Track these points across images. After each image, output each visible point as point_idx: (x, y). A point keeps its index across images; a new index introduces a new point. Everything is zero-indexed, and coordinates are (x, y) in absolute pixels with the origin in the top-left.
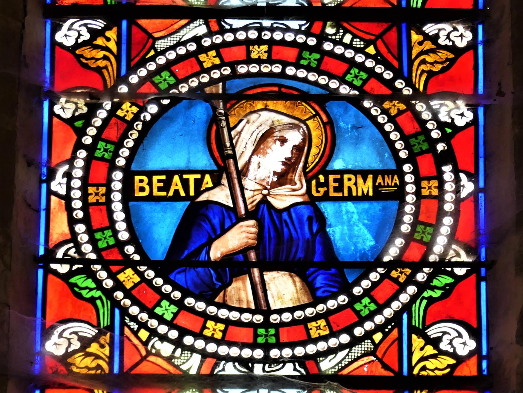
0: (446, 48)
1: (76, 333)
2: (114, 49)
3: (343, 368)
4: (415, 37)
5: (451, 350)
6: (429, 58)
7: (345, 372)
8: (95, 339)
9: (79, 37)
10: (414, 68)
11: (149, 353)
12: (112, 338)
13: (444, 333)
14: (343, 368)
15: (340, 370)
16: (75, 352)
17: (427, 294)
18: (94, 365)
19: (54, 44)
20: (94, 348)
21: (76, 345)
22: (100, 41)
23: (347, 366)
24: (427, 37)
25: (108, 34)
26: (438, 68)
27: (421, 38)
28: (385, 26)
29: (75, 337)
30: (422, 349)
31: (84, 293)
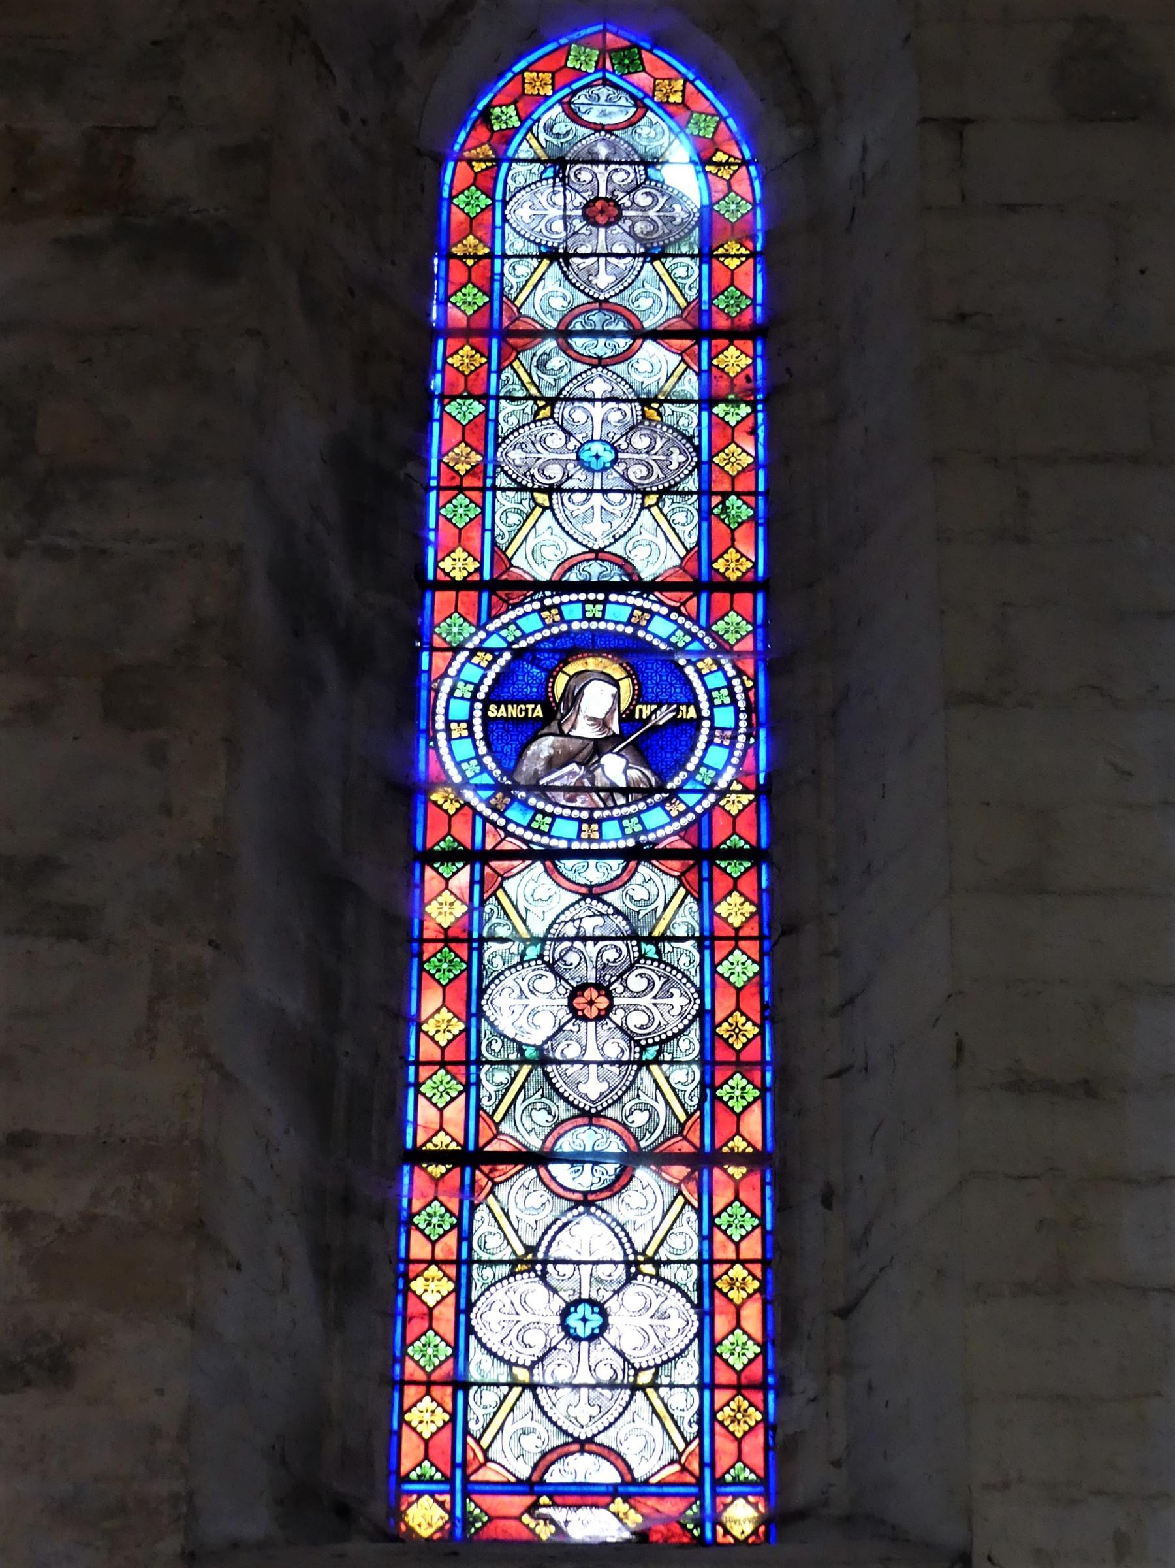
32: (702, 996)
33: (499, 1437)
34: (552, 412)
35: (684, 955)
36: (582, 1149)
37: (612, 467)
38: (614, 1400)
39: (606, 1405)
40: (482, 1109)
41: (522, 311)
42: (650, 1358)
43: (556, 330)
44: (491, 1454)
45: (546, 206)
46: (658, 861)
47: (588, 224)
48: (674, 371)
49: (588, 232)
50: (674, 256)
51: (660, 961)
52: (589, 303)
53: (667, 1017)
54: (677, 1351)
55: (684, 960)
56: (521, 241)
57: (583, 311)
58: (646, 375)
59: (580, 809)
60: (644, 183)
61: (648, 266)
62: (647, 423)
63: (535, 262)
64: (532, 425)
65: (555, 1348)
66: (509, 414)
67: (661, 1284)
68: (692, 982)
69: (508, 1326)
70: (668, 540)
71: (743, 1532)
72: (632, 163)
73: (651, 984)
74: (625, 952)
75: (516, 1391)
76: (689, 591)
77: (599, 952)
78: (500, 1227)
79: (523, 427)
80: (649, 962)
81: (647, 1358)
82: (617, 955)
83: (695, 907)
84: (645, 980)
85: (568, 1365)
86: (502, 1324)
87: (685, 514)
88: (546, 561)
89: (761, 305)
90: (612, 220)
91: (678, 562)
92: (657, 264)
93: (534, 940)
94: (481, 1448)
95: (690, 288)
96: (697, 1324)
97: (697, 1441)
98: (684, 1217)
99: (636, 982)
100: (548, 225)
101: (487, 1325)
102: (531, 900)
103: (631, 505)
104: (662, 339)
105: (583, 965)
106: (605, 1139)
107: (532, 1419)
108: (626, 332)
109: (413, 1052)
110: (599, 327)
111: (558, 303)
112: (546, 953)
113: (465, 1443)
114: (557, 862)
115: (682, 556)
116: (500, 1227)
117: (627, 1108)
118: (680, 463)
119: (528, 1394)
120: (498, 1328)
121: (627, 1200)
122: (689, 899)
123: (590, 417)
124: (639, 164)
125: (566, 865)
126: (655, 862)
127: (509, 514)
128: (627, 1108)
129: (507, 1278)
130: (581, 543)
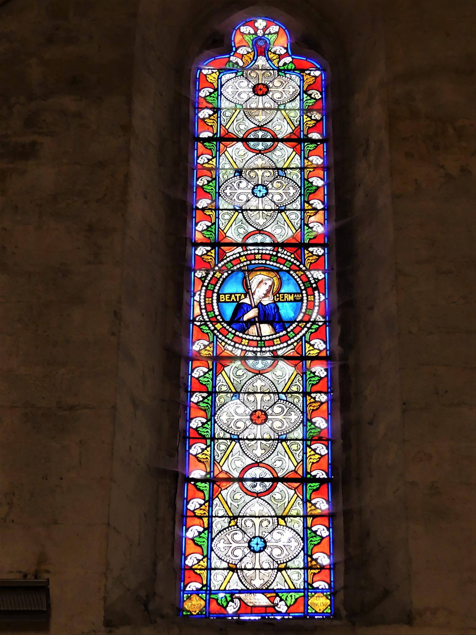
0: (314, 120)
1: (202, 343)
2: (214, 256)
3: (285, 354)
4: (306, 252)
5: (318, 348)
6: (313, 457)
7: (285, 355)
9: (202, 275)
10: (306, 261)
11: (225, 350)
14: (285, 354)
15: (284, 354)
17: (310, 331)
23: (286, 353)
27: (306, 96)
28: (297, 248)
31: (205, 331)
32: (301, 190)
33: (230, 229)
35: (296, 523)
36: (255, 477)
37: (266, 196)
38: (269, 577)
40: (220, 228)
41: (223, 468)
45: (234, 414)
46: (286, 483)
47: (255, 94)
48: (290, 155)
50: (290, 210)
52: (254, 231)
53: (290, 551)
54: (295, 555)
56: (223, 432)
57: (253, 130)
58: (279, 157)
60: (278, 401)
61: (279, 573)
62: (279, 177)
67: (287, 528)
68: (299, 409)
70: (289, 458)
71: (320, 610)
73: (283, 410)
74: (272, 173)
77: (260, 522)
80: (282, 77)
81: (283, 559)
82: (270, 398)
83: (299, 158)
84: (281, 409)
85: (251, 563)
86: (225, 548)
87: (295, 215)
90: (264, 93)
92: (283, 213)
95: (296, 121)
96: (302, 544)
97: (300, 229)
99: (277, 409)
101: (219, 549)
102: (235, 375)
103: (273, 523)
104: (286, 142)
105: (257, 177)
106: (264, 473)
107: (237, 586)
108: (272, 357)
110: (259, 483)
114: (244, 482)
120: (223, 550)
121: (275, 153)
122: (297, 155)
123: (257, 175)
124: (274, 517)
127: (225, 215)
130: (254, 123)
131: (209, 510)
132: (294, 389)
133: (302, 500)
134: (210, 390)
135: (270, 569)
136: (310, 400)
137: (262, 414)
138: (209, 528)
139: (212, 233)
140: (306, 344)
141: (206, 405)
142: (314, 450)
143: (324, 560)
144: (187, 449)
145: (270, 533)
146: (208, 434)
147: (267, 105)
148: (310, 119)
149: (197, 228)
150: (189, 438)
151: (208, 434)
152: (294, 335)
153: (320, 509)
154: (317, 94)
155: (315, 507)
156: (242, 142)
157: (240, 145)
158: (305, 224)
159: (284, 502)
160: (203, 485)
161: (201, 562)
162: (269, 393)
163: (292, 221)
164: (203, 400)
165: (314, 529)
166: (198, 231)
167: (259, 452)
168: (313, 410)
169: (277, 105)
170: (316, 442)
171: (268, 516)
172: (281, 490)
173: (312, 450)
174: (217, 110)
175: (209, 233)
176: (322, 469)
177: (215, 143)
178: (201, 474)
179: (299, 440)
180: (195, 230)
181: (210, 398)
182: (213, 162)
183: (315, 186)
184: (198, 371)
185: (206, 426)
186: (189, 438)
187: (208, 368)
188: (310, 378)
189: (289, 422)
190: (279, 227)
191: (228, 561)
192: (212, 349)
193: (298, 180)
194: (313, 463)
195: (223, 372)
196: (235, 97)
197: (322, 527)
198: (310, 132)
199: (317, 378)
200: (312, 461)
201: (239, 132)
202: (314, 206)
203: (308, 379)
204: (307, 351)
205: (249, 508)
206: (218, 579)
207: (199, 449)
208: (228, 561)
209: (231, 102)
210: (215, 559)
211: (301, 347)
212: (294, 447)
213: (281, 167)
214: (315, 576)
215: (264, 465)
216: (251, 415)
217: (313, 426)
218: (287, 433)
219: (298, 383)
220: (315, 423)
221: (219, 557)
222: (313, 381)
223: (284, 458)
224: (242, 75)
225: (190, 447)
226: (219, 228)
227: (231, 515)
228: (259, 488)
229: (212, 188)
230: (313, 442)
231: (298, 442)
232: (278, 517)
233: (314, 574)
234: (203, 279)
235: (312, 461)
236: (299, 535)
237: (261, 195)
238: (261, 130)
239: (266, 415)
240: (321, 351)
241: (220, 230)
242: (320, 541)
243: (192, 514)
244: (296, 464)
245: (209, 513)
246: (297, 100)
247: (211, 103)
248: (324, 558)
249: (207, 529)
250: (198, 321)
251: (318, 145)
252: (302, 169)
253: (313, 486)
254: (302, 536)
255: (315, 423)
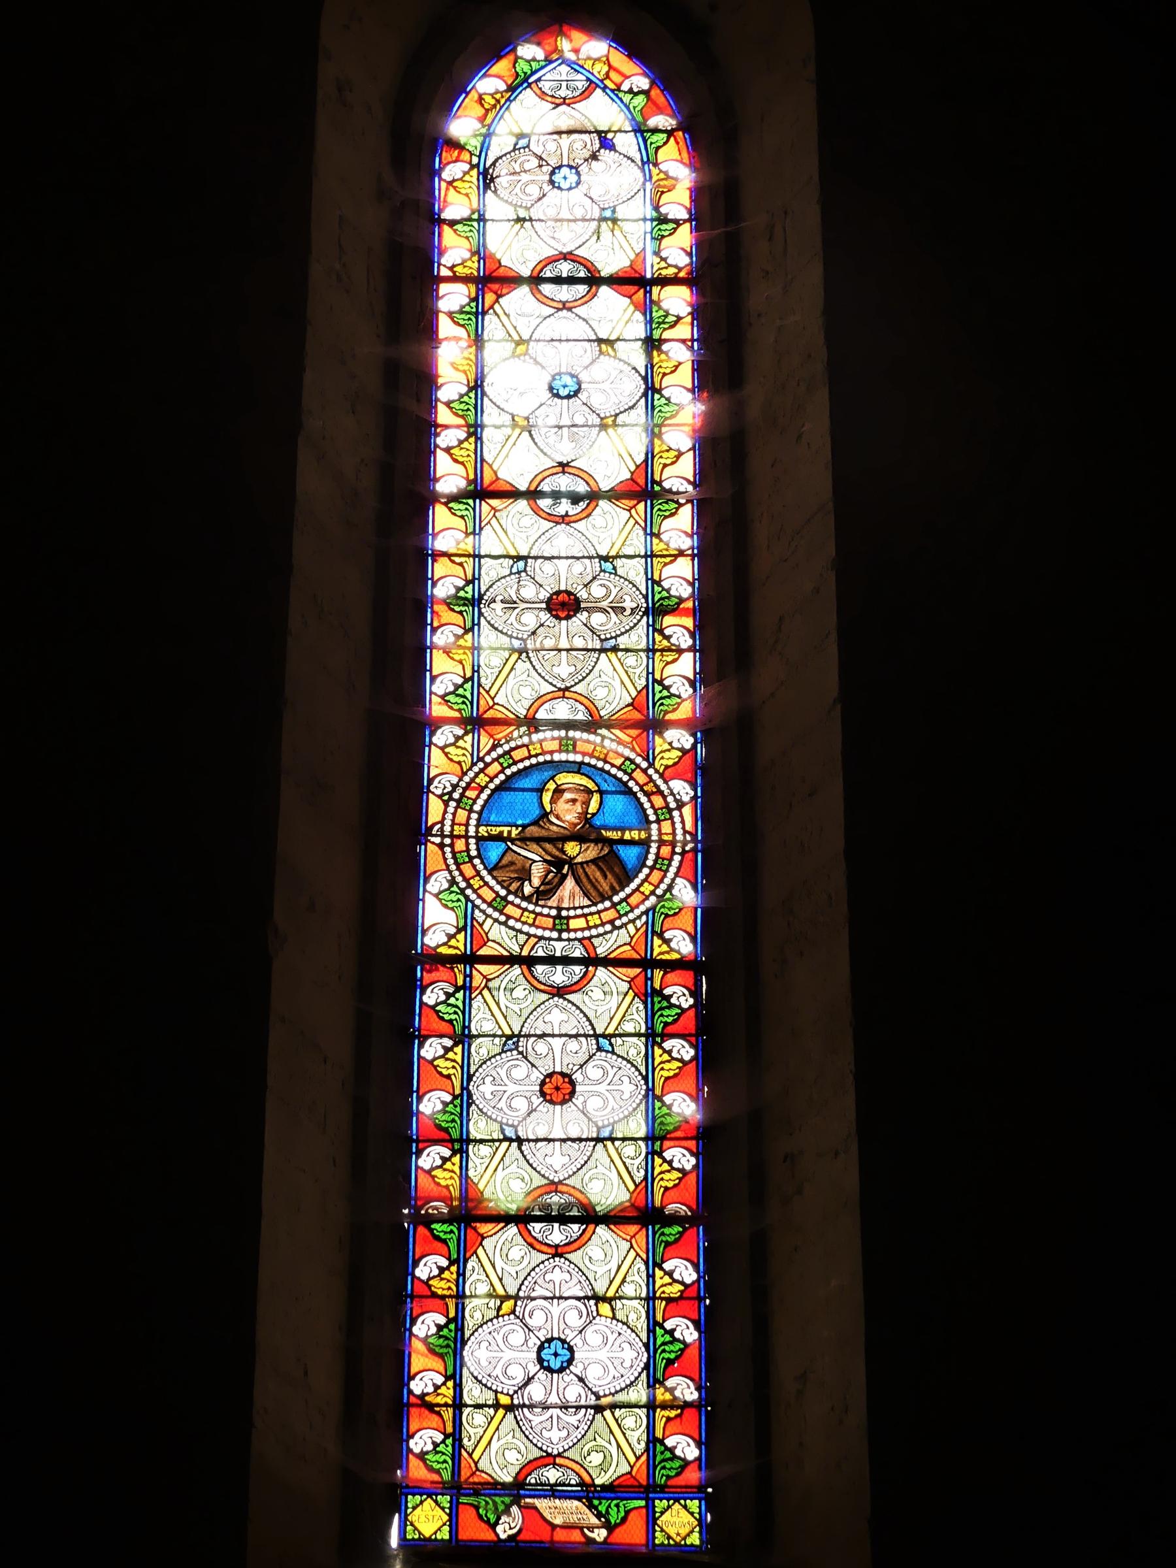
0: (678, 1170)
5: (679, 1057)
6: (667, 1066)
7: (612, 956)
8: (448, 1268)
10: (658, 1356)
11: (488, 940)
12: (462, 1101)
13: (678, 1384)
16: (434, 1277)
17: (662, 326)
18: (446, 1286)
19: (417, 1167)
20: (446, 1275)
21: (436, 1272)
22: (460, 691)
23: (613, 951)
24: (665, 1051)
25: (456, 1049)
26: (671, 1073)
28: (635, 502)
29: (441, 992)
30: (660, 1166)
31: (457, 512)
33: (504, 686)
34: (527, 350)
39: (574, 1154)
42: (612, 410)
43: (530, 277)
44: (480, 1466)
49: (552, 625)
51: (616, 574)
55: (633, 1052)
59: (551, 908)
63: (492, 1411)
64: (495, 1320)
65: (535, 1110)
66: (491, 570)
69: (494, 1362)
72: (590, 558)
75: (501, 1412)
76: (639, 967)
78: (493, 1015)
79: (486, 1323)
88: (510, 1466)
89: (701, 797)
91: (628, 476)
93: (507, 1297)
94: (473, 1460)
98: (634, 534)
100: (509, 1101)
104: (615, 1224)
109: (409, 1287)
111: (512, 1456)
112: (518, 1309)
113: (479, 693)
115: (632, 470)
116: (493, 1015)
117: (586, 1449)
118: (632, 609)
119: (526, 434)
125: (540, 969)
126: (612, 1227)
128: (586, 1449)
129: (500, 1054)
131: (457, 1281)
132: (629, 1027)
133: (646, 1263)
134: (458, 1030)
135: (587, 426)
136: (661, 1056)
137: (564, 1082)
138: (458, 1321)
139: (453, 1174)
140: (655, 938)
141: (462, 699)
142: (670, 1274)
143: (686, 1390)
144: (408, 1326)
145: (586, 368)
146: (446, 1468)
147: (579, 420)
148: (669, 1168)
149: (434, 689)
150: (412, 1297)
151: (446, 1468)
152: (628, 908)
153: (678, 952)
154: (684, 995)
155: (669, 1002)
156: (516, 1225)
157: (522, 504)
158: (654, 680)
159: (608, 1007)
160: (445, 1227)
161: (447, 1272)
162: (576, 1036)
163: (630, 670)
164: (448, 998)
165: (668, 1325)
166: (430, 893)
167: (564, 670)
168: (667, 1079)
169: (595, 1129)
170: (677, 1143)
171: (584, 557)
172: (603, 982)
173: (666, 1332)
174: (464, 1038)
175: (460, 752)
176: (688, 1374)
177: (471, 502)
178: (437, 1322)
179: (640, 1407)
180: (431, 693)
181: (458, 1049)
182: (456, 1054)
183: (675, 597)
184: (435, 990)
185: (441, 1448)
186: (412, 1297)
187: (449, 1259)
188: (661, 698)
189: (618, 1098)
190: (603, 684)
191: (514, 202)
192: (458, 1109)
193: (639, 1060)
194: (666, 1189)
195: (480, 1251)
196: (514, 192)
197: (678, 990)
198: (669, 1255)
199: (677, 1464)
200: (664, 1185)
201: (519, 704)
202: (673, 640)
203: (660, 1463)
204: (656, 1173)
205: (541, 1018)
206: (476, 1422)
207: (437, 1157)
208: (499, 1119)
209: (501, 632)
210: (475, 1115)
211: (643, 939)
212: (629, 1422)
213: (604, 554)
214: (668, 1424)
215: (575, 696)
216: (543, 1084)
217: (665, 693)
218: (615, 637)
219: (636, 1016)
220: (670, 940)
221: (476, 1378)
222: (667, 1016)
223: (607, 1445)
224: (513, 1312)
225: (413, 1321)
226: (479, 685)
227: (501, 1292)
228: (565, 507)
229: (449, 1284)
230: (667, 1144)
231: (636, 1410)
232: (596, 1036)
233: (669, 1419)
234: (446, 798)
235: (663, 1184)
236: (637, 371)
237: (558, 1365)
238: (557, 1246)
239: (573, 1083)
240: (680, 269)
241: (481, 690)
242: (677, 1181)
243: (450, 274)
244: (632, 1459)
245: (457, 1286)
246: (641, 1383)
247: (438, 1472)
248: (687, 1268)
249: (455, 1319)
250: (436, 836)
251: (685, 1229)
252: (650, 556)
253: (665, 511)
254: (644, 1073)
255: (670, 940)
